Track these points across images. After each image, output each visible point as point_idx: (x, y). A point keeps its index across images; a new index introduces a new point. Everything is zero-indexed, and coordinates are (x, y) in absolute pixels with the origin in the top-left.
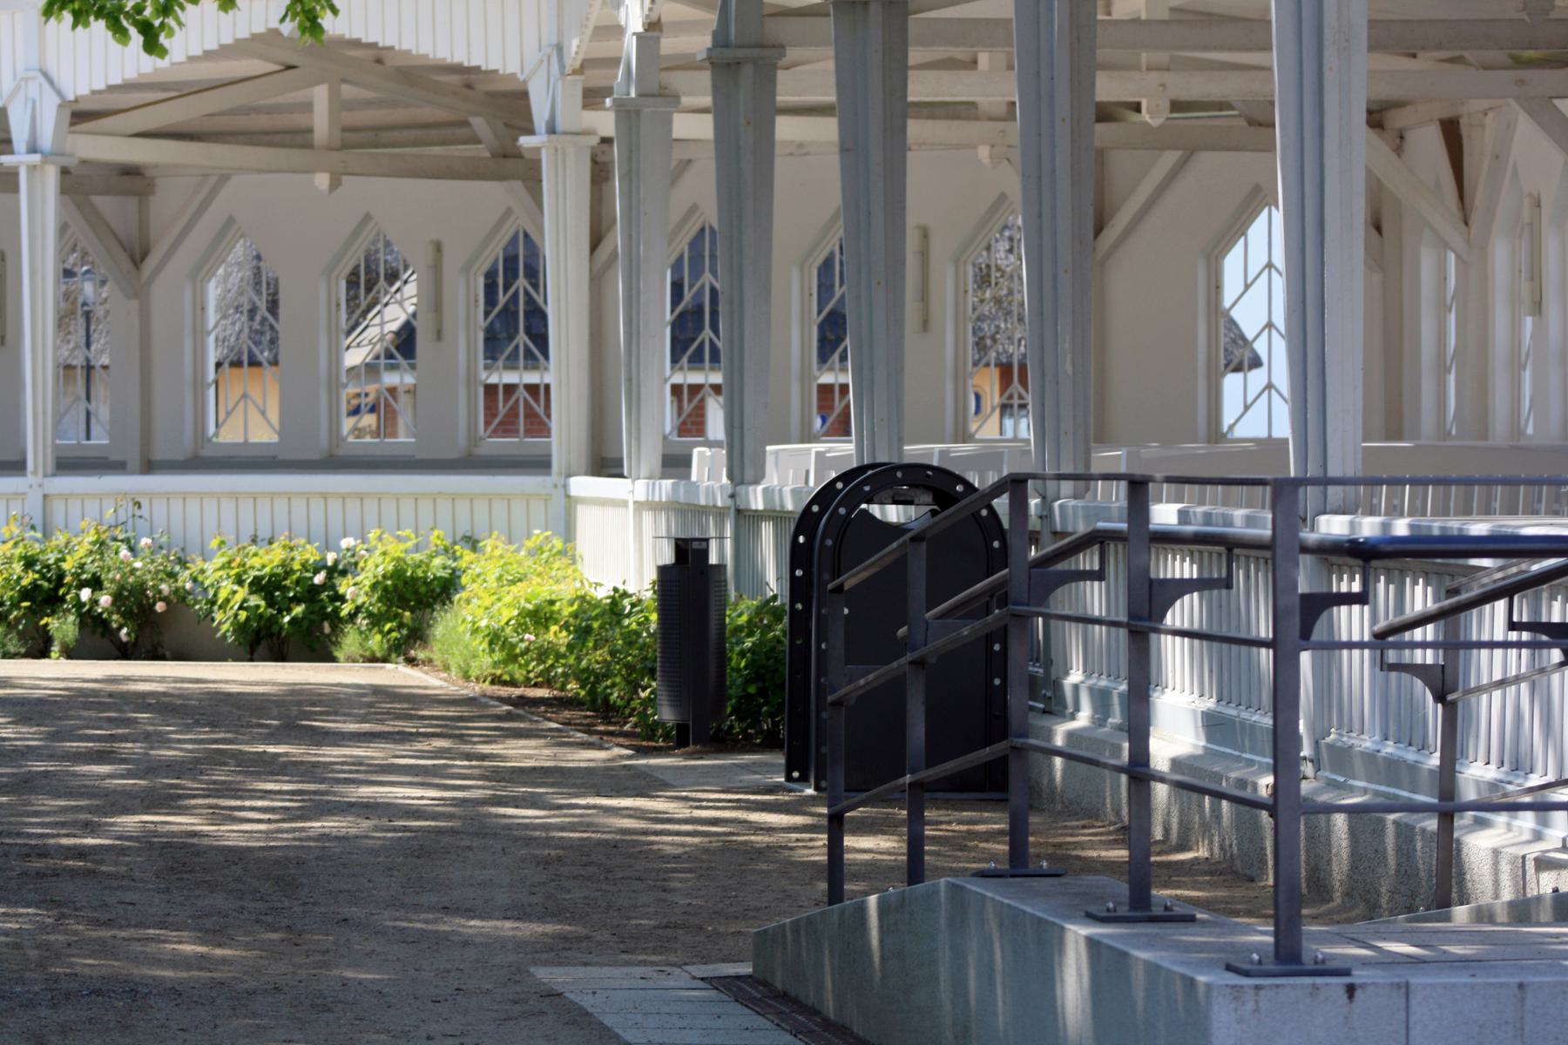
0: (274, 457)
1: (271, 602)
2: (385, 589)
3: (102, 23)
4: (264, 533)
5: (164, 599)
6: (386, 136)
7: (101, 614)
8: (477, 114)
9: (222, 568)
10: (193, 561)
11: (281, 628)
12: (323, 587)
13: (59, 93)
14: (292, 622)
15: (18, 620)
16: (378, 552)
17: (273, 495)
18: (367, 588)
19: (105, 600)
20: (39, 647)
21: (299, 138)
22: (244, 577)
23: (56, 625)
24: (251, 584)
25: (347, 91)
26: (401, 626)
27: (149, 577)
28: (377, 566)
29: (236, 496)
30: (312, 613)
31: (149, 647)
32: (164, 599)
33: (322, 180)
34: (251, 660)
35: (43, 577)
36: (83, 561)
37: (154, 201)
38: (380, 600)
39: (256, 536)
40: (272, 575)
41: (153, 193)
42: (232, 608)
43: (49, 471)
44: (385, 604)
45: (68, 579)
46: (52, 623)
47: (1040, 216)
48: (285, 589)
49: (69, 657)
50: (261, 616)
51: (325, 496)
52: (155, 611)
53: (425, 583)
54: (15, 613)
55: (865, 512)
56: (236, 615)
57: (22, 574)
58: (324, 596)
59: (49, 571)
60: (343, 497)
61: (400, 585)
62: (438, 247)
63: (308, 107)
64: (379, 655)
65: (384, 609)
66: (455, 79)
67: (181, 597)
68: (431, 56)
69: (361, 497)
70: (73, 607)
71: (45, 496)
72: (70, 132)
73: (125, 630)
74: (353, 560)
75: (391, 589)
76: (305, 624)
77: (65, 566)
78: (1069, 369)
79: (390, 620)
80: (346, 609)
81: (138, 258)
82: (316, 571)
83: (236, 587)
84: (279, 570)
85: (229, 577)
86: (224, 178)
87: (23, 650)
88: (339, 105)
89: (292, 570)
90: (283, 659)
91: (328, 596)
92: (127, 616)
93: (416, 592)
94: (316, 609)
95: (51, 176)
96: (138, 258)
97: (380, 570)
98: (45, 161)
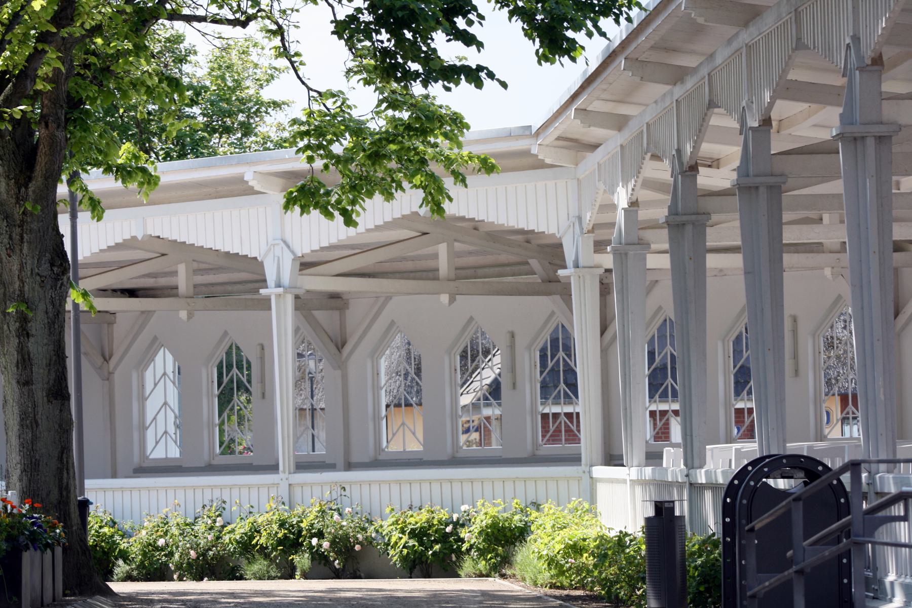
0: (421, 459)
1: (421, 543)
2: (487, 534)
3: (318, 211)
4: (416, 504)
5: (360, 543)
7: (324, 552)
9: (393, 524)
11: (428, 558)
12: (451, 534)
13: (293, 252)
16: (482, 513)
19: (326, 544)
20: (289, 573)
26: (497, 555)
27: (351, 530)
28: (482, 521)
29: (399, 482)
30: (445, 549)
32: (360, 543)
33: (445, 298)
35: (290, 532)
37: (347, 312)
38: (484, 541)
40: (421, 528)
41: (348, 308)
42: (399, 547)
43: (292, 471)
45: (304, 533)
46: (296, 558)
47: (862, 308)
48: (429, 535)
49: (306, 578)
51: (451, 481)
53: (510, 530)
55: (765, 483)
56: (401, 551)
58: (451, 539)
61: (496, 532)
62: (513, 335)
64: (484, 573)
66: (520, 237)
67: (369, 541)
68: (506, 225)
69: (472, 481)
73: (337, 562)
75: (490, 534)
76: (441, 555)
77: (303, 525)
78: (882, 398)
80: (465, 547)
81: (340, 346)
82: (447, 525)
86: (388, 298)
88: (453, 255)
89: (433, 524)
92: (339, 553)
93: (505, 536)
95: (289, 300)
96: (340, 346)
97: (484, 524)
98: (286, 292)
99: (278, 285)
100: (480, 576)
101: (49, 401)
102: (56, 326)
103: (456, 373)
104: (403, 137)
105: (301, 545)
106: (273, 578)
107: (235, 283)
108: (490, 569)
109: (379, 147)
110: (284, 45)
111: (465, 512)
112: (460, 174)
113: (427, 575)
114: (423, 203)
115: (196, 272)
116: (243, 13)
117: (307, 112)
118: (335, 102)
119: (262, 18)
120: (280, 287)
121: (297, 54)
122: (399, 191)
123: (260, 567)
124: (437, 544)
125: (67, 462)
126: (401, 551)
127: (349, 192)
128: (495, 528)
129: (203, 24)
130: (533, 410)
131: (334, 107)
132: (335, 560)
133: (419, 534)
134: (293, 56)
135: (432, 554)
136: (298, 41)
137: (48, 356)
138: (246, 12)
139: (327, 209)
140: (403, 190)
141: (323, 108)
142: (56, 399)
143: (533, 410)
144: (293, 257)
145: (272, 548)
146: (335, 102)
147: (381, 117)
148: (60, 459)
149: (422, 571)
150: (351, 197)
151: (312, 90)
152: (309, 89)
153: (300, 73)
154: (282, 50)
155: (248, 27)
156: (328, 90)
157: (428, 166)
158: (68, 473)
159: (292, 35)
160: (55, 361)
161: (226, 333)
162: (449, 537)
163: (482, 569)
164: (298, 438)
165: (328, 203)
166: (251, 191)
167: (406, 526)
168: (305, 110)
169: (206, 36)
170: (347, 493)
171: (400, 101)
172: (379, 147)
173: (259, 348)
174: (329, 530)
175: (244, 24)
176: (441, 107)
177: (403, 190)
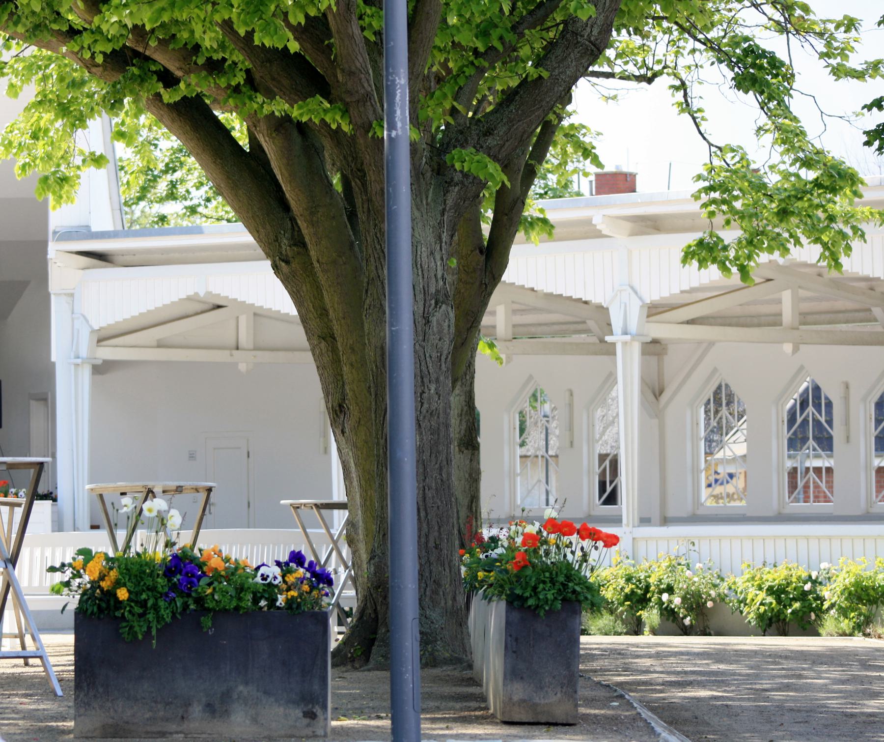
0: (744, 515)
1: (779, 601)
2: (850, 593)
3: (715, 266)
4: (770, 560)
5: (713, 600)
6: (810, 318)
7: (674, 609)
8: (876, 306)
9: (748, 581)
10: (728, 577)
11: (786, 616)
12: (810, 592)
13: (640, 299)
14: (792, 613)
15: (622, 612)
16: (844, 571)
17: (775, 538)
18: (839, 593)
19: (677, 600)
20: (636, 628)
21: (775, 320)
22: (763, 586)
23: (647, 615)
24: (767, 590)
25: (802, 293)
26: (860, 615)
27: (703, 586)
28: (845, 579)
29: (752, 538)
30: (804, 607)
31: (702, 629)
32: (713, 600)
33: (788, 348)
34: (764, 636)
35: (637, 587)
36: (661, 577)
37: (666, 358)
38: (846, 599)
39: (765, 562)
40: (780, 585)
41: (666, 354)
42: (756, 604)
43: (636, 524)
44: (848, 602)
45: (652, 588)
46: (644, 614)
48: (787, 593)
49: (655, 634)
50: (773, 609)
51: (807, 538)
52: (707, 606)
53: (873, 589)
54: (621, 608)
56: (758, 609)
57: (625, 585)
58: (810, 597)
59: (640, 584)
60: (819, 538)
61: (859, 590)
62: (847, 387)
63: (779, 301)
64: (847, 632)
65: (848, 604)
66: (863, 285)
67: (722, 598)
68: (850, 271)
69: (830, 538)
70: (656, 604)
71: (634, 539)
72: (648, 322)
73: (689, 618)
74: (827, 576)
75: (854, 592)
76: (800, 614)
77: (651, 580)
79: (852, 611)
80: (826, 605)
81: (657, 394)
82: (805, 583)
83: (758, 592)
84: (784, 582)
85: (753, 585)
86: (711, 344)
87: (625, 631)
88: (796, 300)
89: (791, 581)
90: (785, 635)
91: (813, 597)
92: (690, 609)
93: (868, 595)
94: (807, 605)
95: (636, 348)
96: (657, 394)
97: (847, 582)
98: (633, 339)
99: (625, 333)
100: (841, 635)
101: (460, 451)
102: (468, 377)
103: (783, 424)
104: (812, 195)
105: (650, 600)
106: (620, 634)
107: (540, 325)
108: (854, 628)
109: (788, 204)
110: (686, 101)
111: (824, 570)
112: (859, 229)
113: (784, 633)
114: (820, 258)
115: (514, 312)
116: (648, 69)
117: (707, 167)
118: (733, 157)
119: (668, 74)
120: (626, 334)
121: (699, 110)
122: (797, 246)
123: (606, 622)
124: (796, 602)
125: (476, 510)
126: (758, 609)
127: (746, 247)
128: (858, 587)
129: (611, 80)
130: (868, 463)
131: (733, 162)
132: (685, 617)
133: (777, 592)
134: (696, 112)
135: (791, 613)
136: (701, 97)
137: (460, 407)
138: (652, 69)
139: (724, 264)
140: (801, 245)
141: (723, 163)
142: (467, 449)
143: (868, 463)
144: (641, 304)
145: (619, 604)
146: (733, 157)
147: (774, 172)
148: (470, 508)
149: (778, 629)
150: (746, 252)
151: (713, 145)
152: (710, 145)
153: (701, 128)
154: (684, 106)
155: (653, 83)
156: (727, 145)
157: (836, 223)
158: (476, 521)
159: (694, 90)
160: (467, 411)
161: (531, 378)
162: (807, 595)
163: (845, 628)
164: (529, 492)
165: (727, 258)
166: (599, 235)
167: (763, 583)
168: (705, 165)
169: (596, 86)
170: (696, 548)
171: (815, 160)
172: (788, 204)
173: (568, 394)
174: (680, 586)
175: (650, 81)
176: (849, 168)
177: (801, 245)
